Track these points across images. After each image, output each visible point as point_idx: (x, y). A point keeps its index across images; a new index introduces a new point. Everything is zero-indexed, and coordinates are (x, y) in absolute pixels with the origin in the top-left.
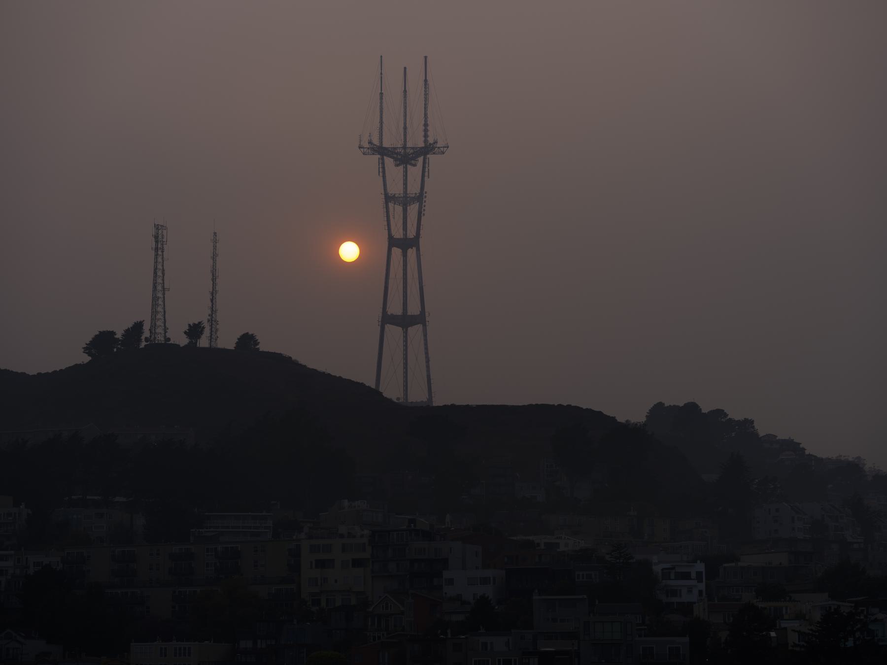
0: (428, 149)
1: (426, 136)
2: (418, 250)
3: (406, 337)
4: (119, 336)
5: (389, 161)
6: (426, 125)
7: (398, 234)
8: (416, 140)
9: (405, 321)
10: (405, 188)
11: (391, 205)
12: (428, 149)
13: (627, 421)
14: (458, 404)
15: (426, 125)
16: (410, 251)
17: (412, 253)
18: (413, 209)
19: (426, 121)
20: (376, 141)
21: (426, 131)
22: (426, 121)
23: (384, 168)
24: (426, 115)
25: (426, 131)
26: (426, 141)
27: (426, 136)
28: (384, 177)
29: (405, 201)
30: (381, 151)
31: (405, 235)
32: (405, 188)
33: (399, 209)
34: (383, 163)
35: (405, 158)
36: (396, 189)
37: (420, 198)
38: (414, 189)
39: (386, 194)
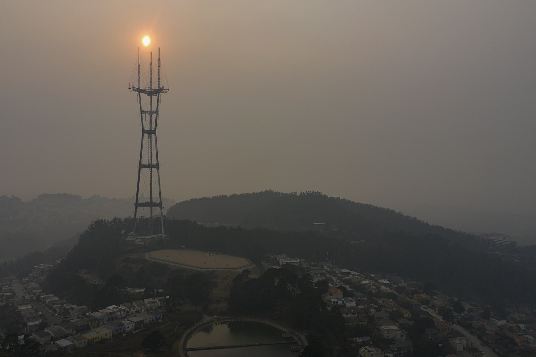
0: (160, 90)
1: (159, 84)
2: (156, 135)
3: (151, 172)
4: (123, 221)
5: (143, 96)
6: (159, 79)
7: (147, 128)
8: (155, 87)
9: (150, 166)
10: (151, 108)
11: (144, 115)
12: (160, 90)
13: (115, 219)
14: (238, 193)
15: (159, 79)
16: (153, 135)
17: (153, 135)
18: (154, 116)
19: (159, 77)
20: (136, 86)
21: (159, 82)
22: (159, 77)
23: (140, 98)
24: (159, 74)
25: (159, 82)
26: (159, 87)
27: (159, 84)
28: (140, 102)
29: (151, 113)
30: (139, 91)
31: (151, 110)
32: (151, 108)
33: (148, 116)
34: (140, 96)
35: (151, 93)
36: (146, 108)
37: (156, 112)
38: (154, 108)
39: (141, 110)
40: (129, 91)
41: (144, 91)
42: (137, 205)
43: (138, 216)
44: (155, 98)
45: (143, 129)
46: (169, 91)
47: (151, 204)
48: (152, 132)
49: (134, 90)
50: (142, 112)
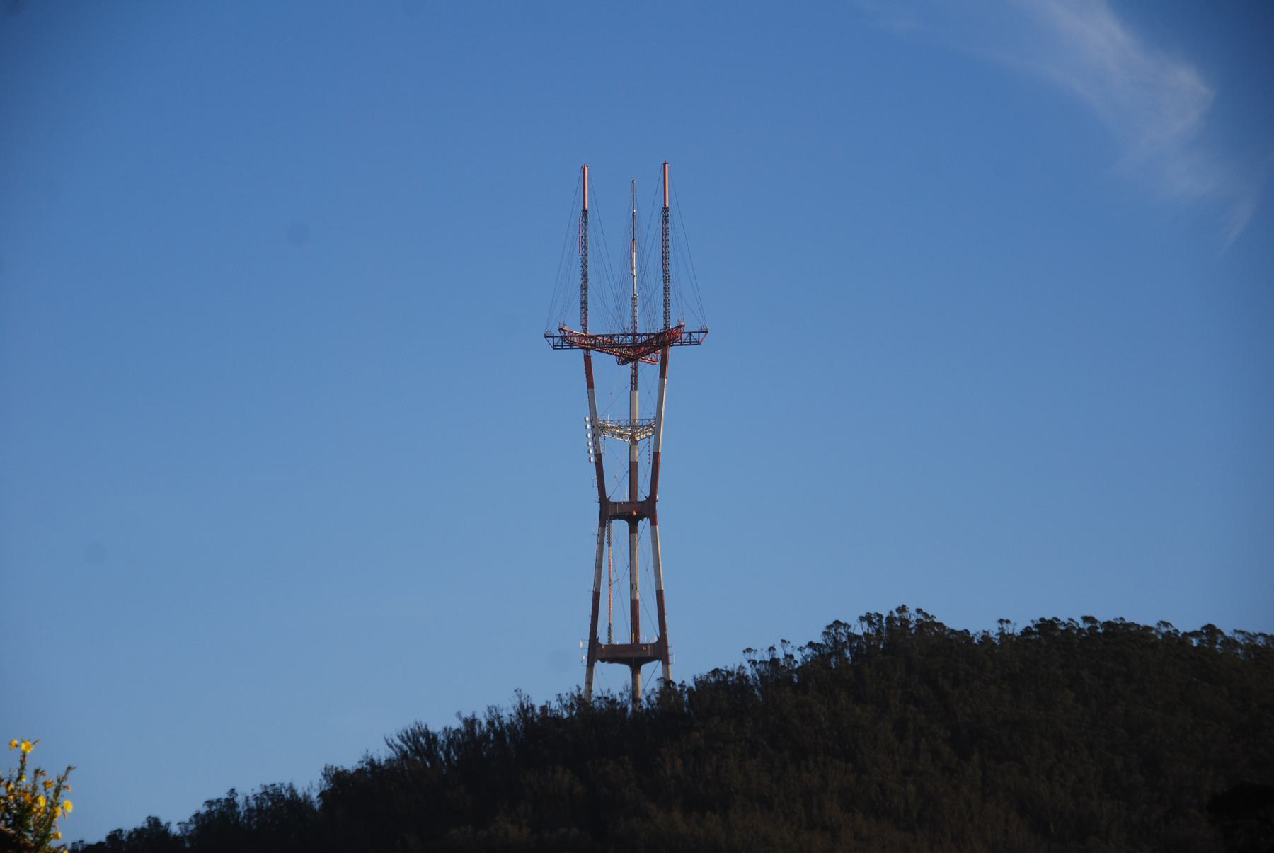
2: (653, 523)
7: (618, 493)
8: (649, 324)
13: (524, 711)
17: (644, 524)
29: (632, 431)
30: (590, 344)
31: (589, 690)
38: (643, 494)
40: (546, 345)
41: (605, 344)
42: (598, 652)
43: (597, 690)
44: (648, 370)
45: (604, 500)
46: (707, 340)
47: (634, 656)
48: (638, 512)
49: (566, 341)
50: (598, 429)
